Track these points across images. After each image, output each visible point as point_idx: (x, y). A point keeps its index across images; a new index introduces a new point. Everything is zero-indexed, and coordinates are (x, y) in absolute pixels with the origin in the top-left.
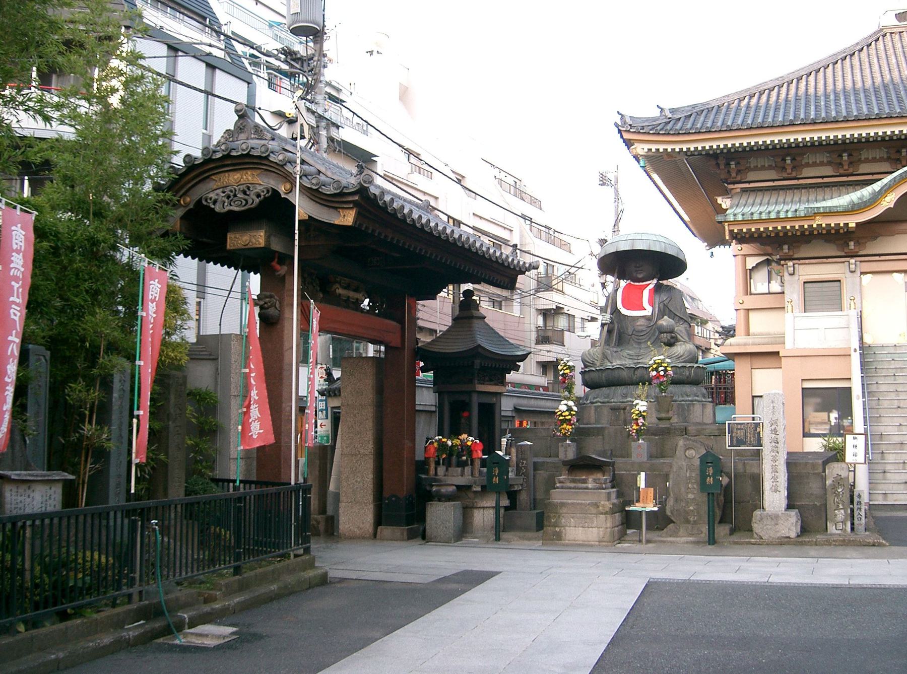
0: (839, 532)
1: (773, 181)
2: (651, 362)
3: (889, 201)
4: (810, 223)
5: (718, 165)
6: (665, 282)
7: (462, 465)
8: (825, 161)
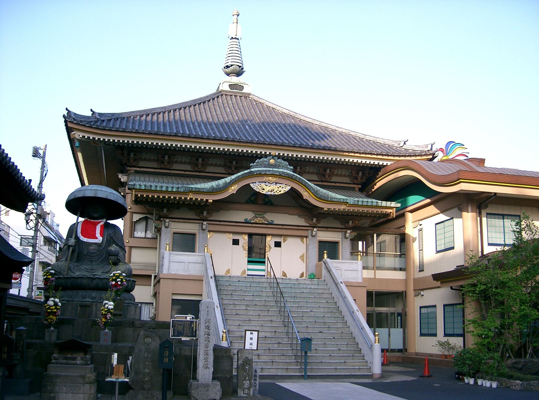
0: (245, 395)
1: (155, 168)
2: (112, 275)
3: (234, 189)
4: (186, 196)
5: (123, 154)
6: (111, 222)
7: (497, 352)
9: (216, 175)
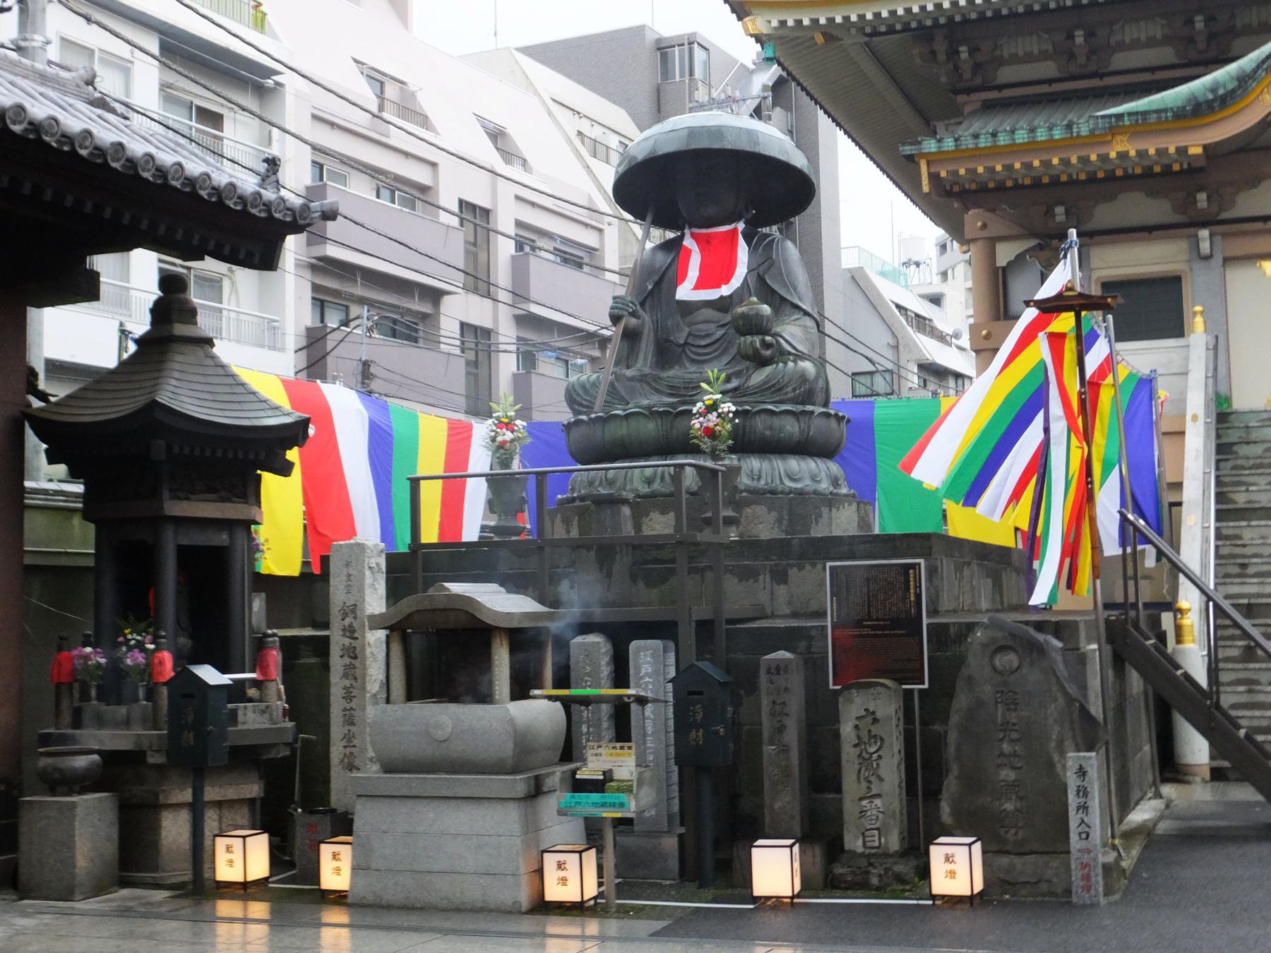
4: (1103, 150)
8: (1159, 36)
9: (1160, 75)
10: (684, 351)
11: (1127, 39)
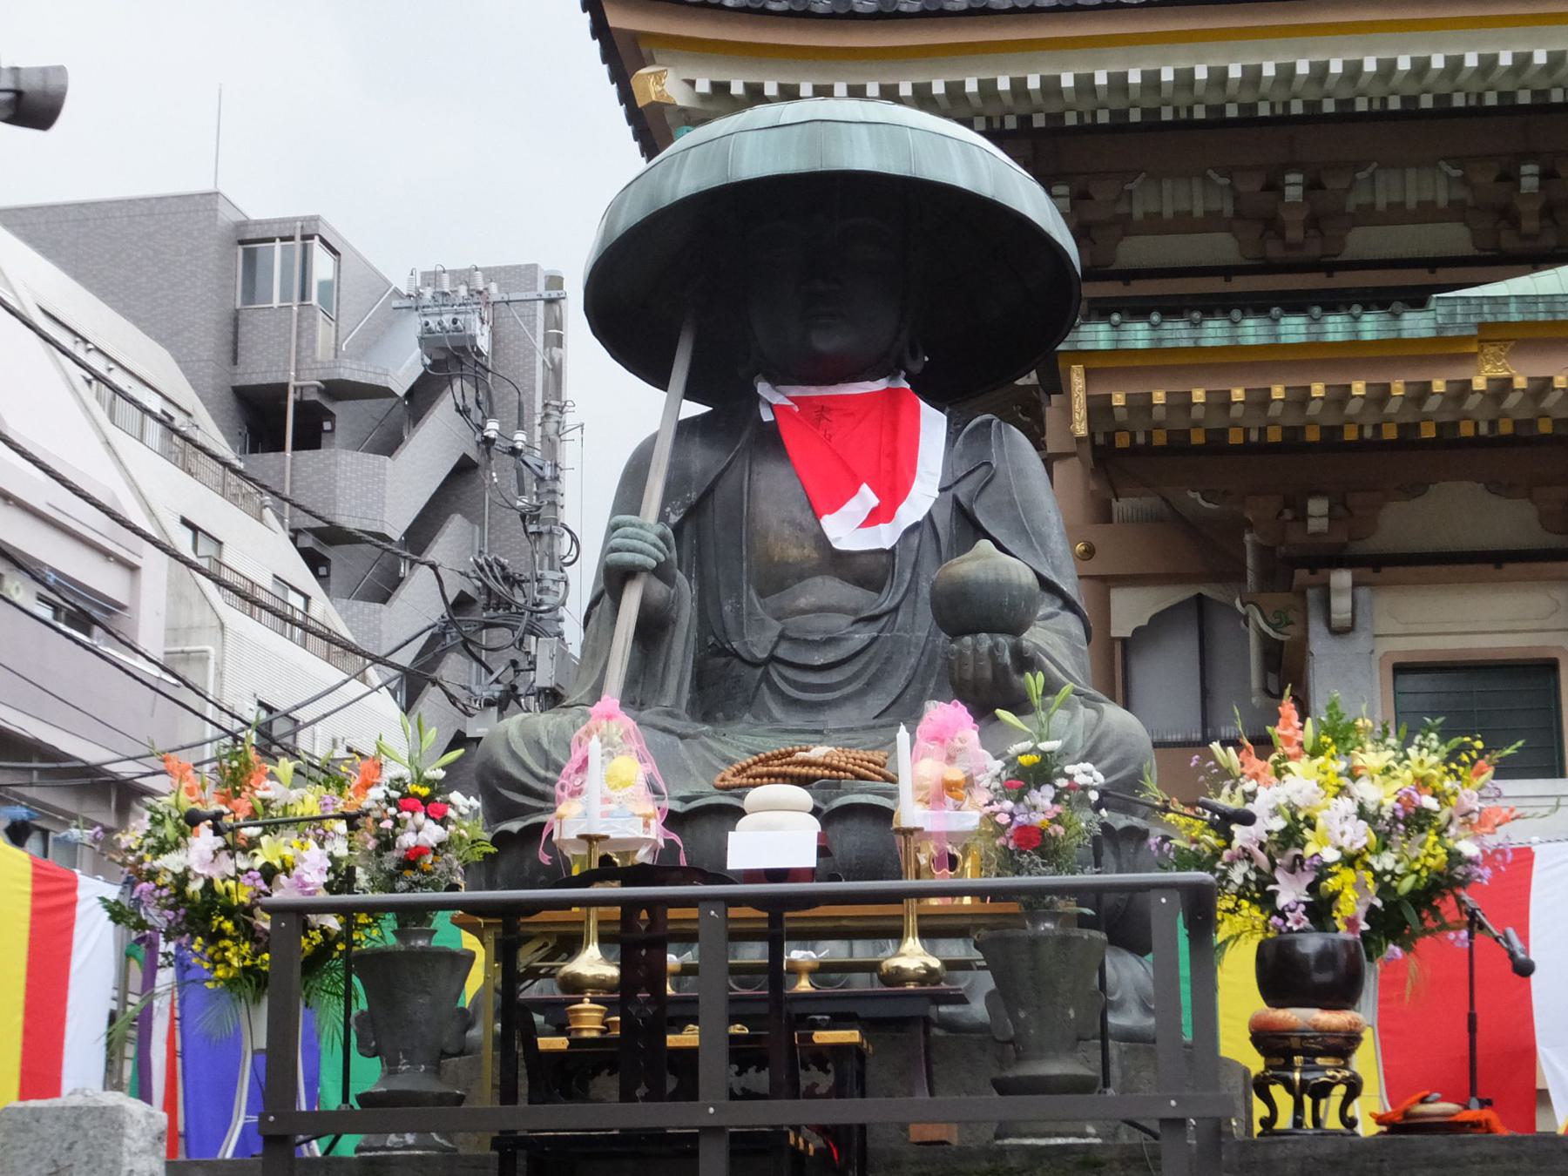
1: (1227, 272)
4: (1459, 373)
10: (766, 677)
11: (1381, 203)
